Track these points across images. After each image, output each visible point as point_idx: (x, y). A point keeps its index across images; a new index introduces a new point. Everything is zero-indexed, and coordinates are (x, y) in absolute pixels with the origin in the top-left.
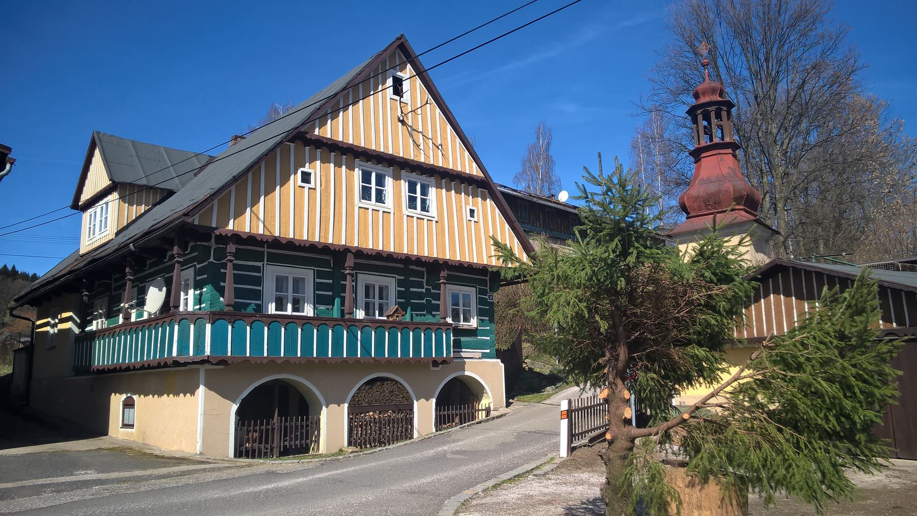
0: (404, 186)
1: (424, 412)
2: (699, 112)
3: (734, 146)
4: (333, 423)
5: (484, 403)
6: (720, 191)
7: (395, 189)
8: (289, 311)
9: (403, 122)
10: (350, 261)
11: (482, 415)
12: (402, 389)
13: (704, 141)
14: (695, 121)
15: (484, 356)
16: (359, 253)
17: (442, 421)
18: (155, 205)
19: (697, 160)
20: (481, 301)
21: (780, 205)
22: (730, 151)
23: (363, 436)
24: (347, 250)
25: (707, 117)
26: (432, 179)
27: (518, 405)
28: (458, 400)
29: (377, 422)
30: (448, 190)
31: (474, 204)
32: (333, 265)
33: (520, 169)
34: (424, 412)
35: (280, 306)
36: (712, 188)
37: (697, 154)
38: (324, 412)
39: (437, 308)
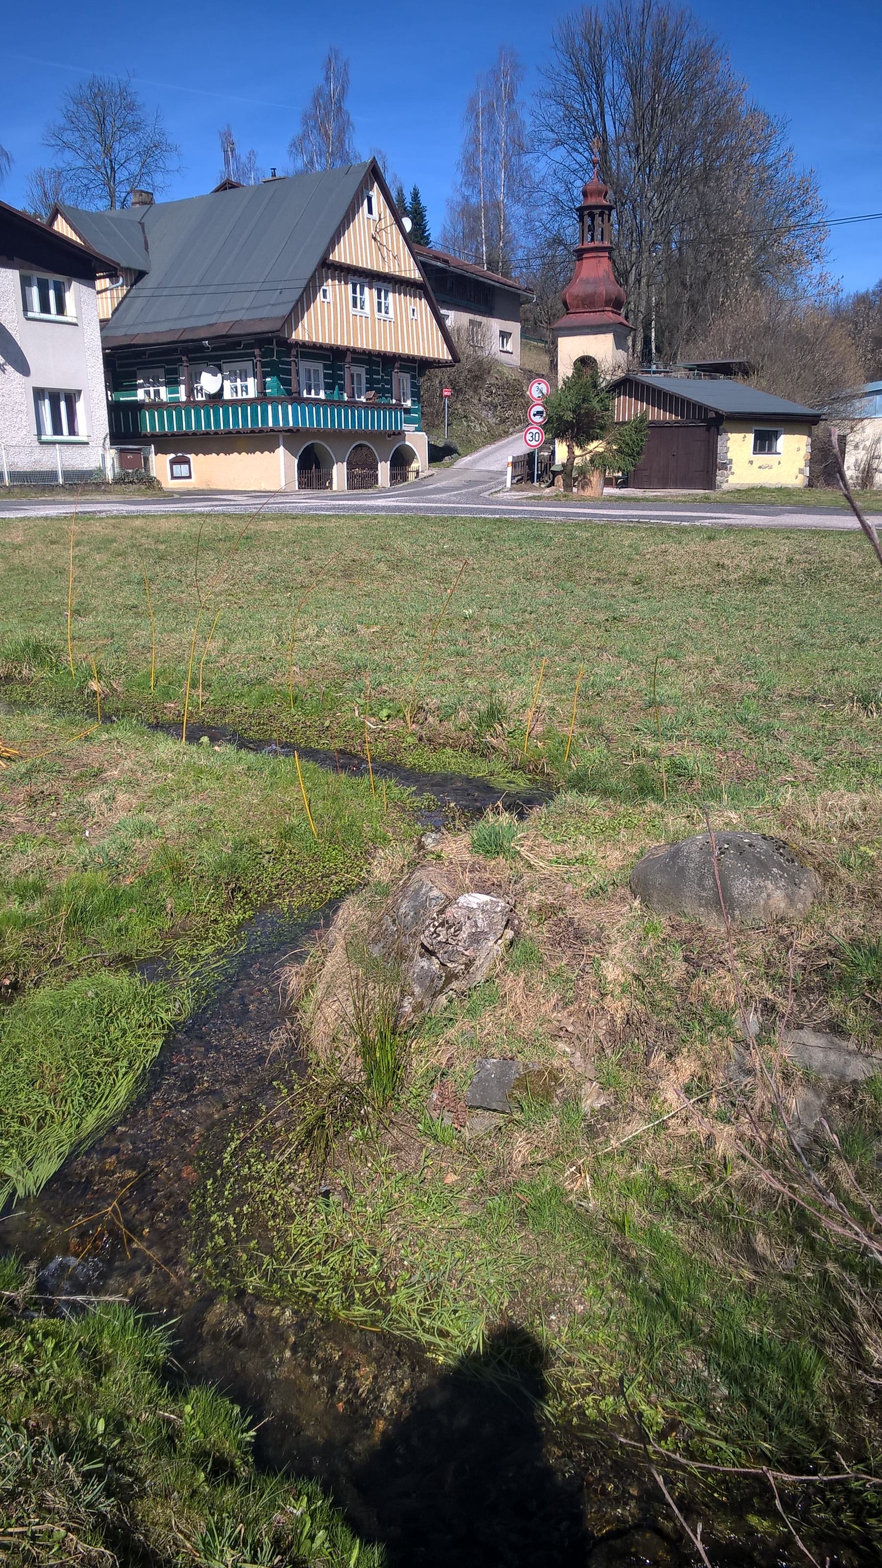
0: (375, 292)
1: (384, 469)
2: (586, 212)
3: (609, 250)
4: (339, 473)
5: (414, 466)
6: (595, 293)
7: (369, 295)
8: (313, 396)
9: (375, 239)
10: (348, 359)
11: (412, 476)
12: (372, 453)
13: (588, 244)
14: (581, 219)
15: (417, 430)
16: (354, 351)
17: (393, 477)
18: (132, 286)
19: (580, 258)
20: (413, 385)
21: (644, 280)
22: (607, 254)
23: (354, 482)
24: (348, 349)
25: (592, 216)
26: (390, 285)
27: (303, 492)
28: (401, 461)
29: (362, 478)
30: (405, 295)
31: (415, 304)
32: (334, 358)
33: (297, 130)
34: (384, 469)
35: (309, 393)
36: (590, 289)
37: (580, 254)
38: (335, 467)
39: (390, 391)
